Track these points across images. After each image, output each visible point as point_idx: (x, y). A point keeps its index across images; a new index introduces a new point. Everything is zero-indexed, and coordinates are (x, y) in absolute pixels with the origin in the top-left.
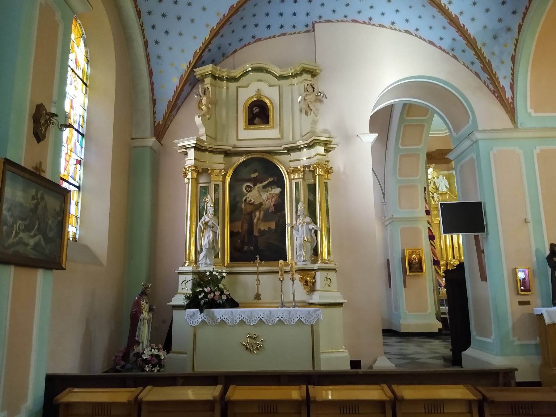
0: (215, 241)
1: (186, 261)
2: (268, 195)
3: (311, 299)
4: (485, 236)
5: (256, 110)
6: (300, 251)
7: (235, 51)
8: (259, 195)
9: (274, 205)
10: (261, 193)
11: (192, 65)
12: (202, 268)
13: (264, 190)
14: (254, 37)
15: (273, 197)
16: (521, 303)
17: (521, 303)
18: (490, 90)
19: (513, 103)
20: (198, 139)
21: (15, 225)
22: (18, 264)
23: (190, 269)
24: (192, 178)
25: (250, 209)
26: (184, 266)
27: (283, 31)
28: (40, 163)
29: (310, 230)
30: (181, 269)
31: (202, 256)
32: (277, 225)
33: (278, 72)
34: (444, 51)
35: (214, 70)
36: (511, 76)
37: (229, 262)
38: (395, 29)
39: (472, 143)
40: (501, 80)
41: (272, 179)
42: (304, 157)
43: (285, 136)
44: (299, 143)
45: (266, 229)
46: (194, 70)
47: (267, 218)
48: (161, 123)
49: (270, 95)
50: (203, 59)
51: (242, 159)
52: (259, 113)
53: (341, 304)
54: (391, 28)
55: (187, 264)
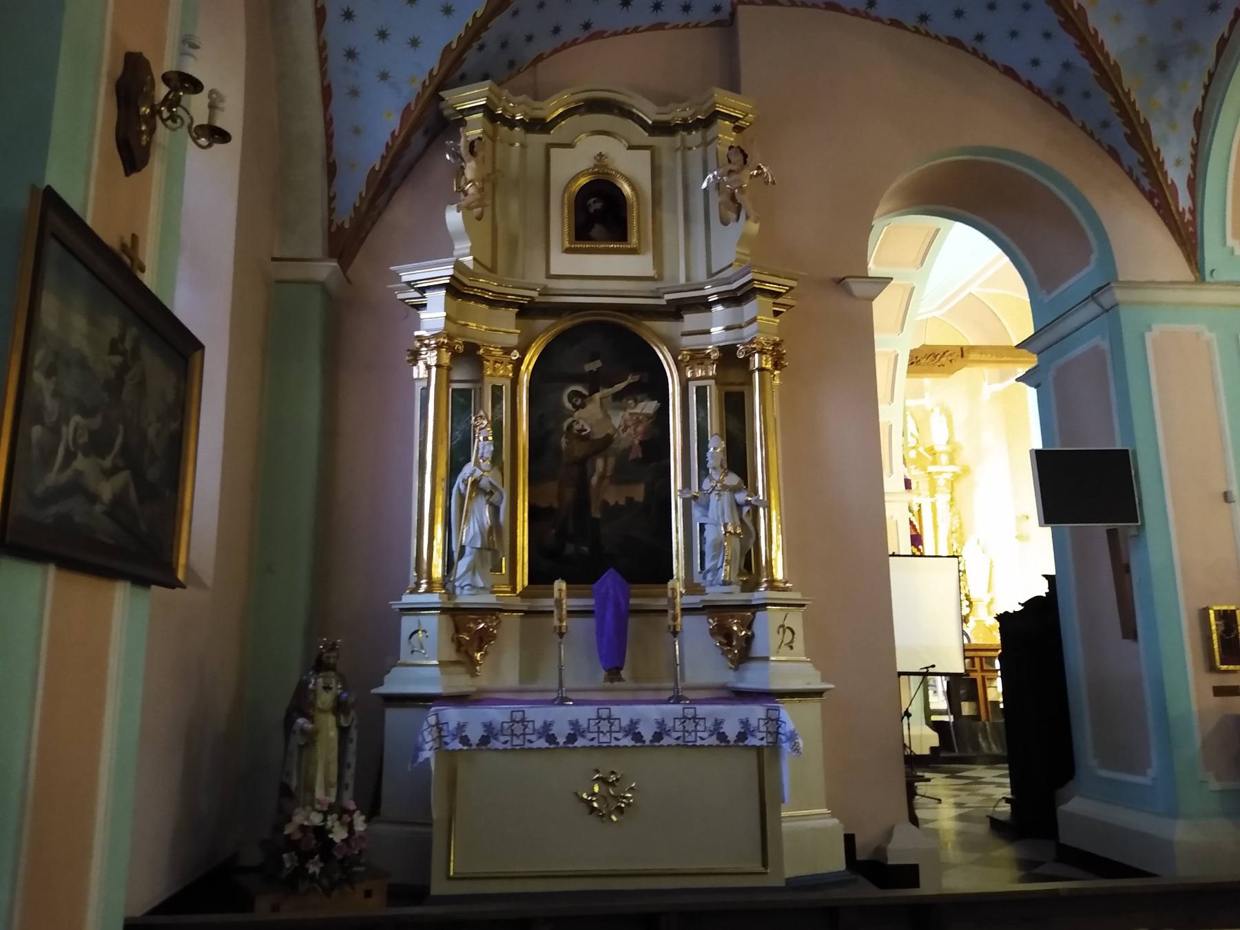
0: (496, 526)
1: (419, 577)
2: (627, 416)
3: (742, 681)
4: (1133, 532)
5: (595, 205)
6: (713, 558)
7: (540, 58)
8: (601, 416)
9: (641, 443)
10: (610, 412)
11: (436, 81)
12: (465, 598)
13: (617, 404)
14: (587, 26)
15: (638, 422)
16: (1219, 691)
17: (1219, 691)
18: (1142, 190)
19: (1193, 223)
20: (458, 266)
21: (64, 428)
22: (67, 563)
23: (435, 598)
24: (437, 366)
25: (579, 450)
26: (414, 591)
27: (660, 17)
28: (134, 238)
29: (739, 507)
30: (408, 599)
31: (462, 566)
32: (649, 493)
33: (650, 113)
34: (1039, 93)
35: (492, 97)
36: (1191, 162)
37: (526, 583)
38: (927, 34)
39: (1099, 310)
40: (1169, 166)
41: (637, 378)
42: (717, 327)
43: (667, 273)
44: (709, 289)
45: (622, 502)
46: (441, 93)
47: (623, 473)
48: (347, 226)
49: (632, 170)
50: (465, 67)
51: (566, 323)
52: (601, 214)
53: (818, 693)
54: (917, 31)
55: (424, 587)
